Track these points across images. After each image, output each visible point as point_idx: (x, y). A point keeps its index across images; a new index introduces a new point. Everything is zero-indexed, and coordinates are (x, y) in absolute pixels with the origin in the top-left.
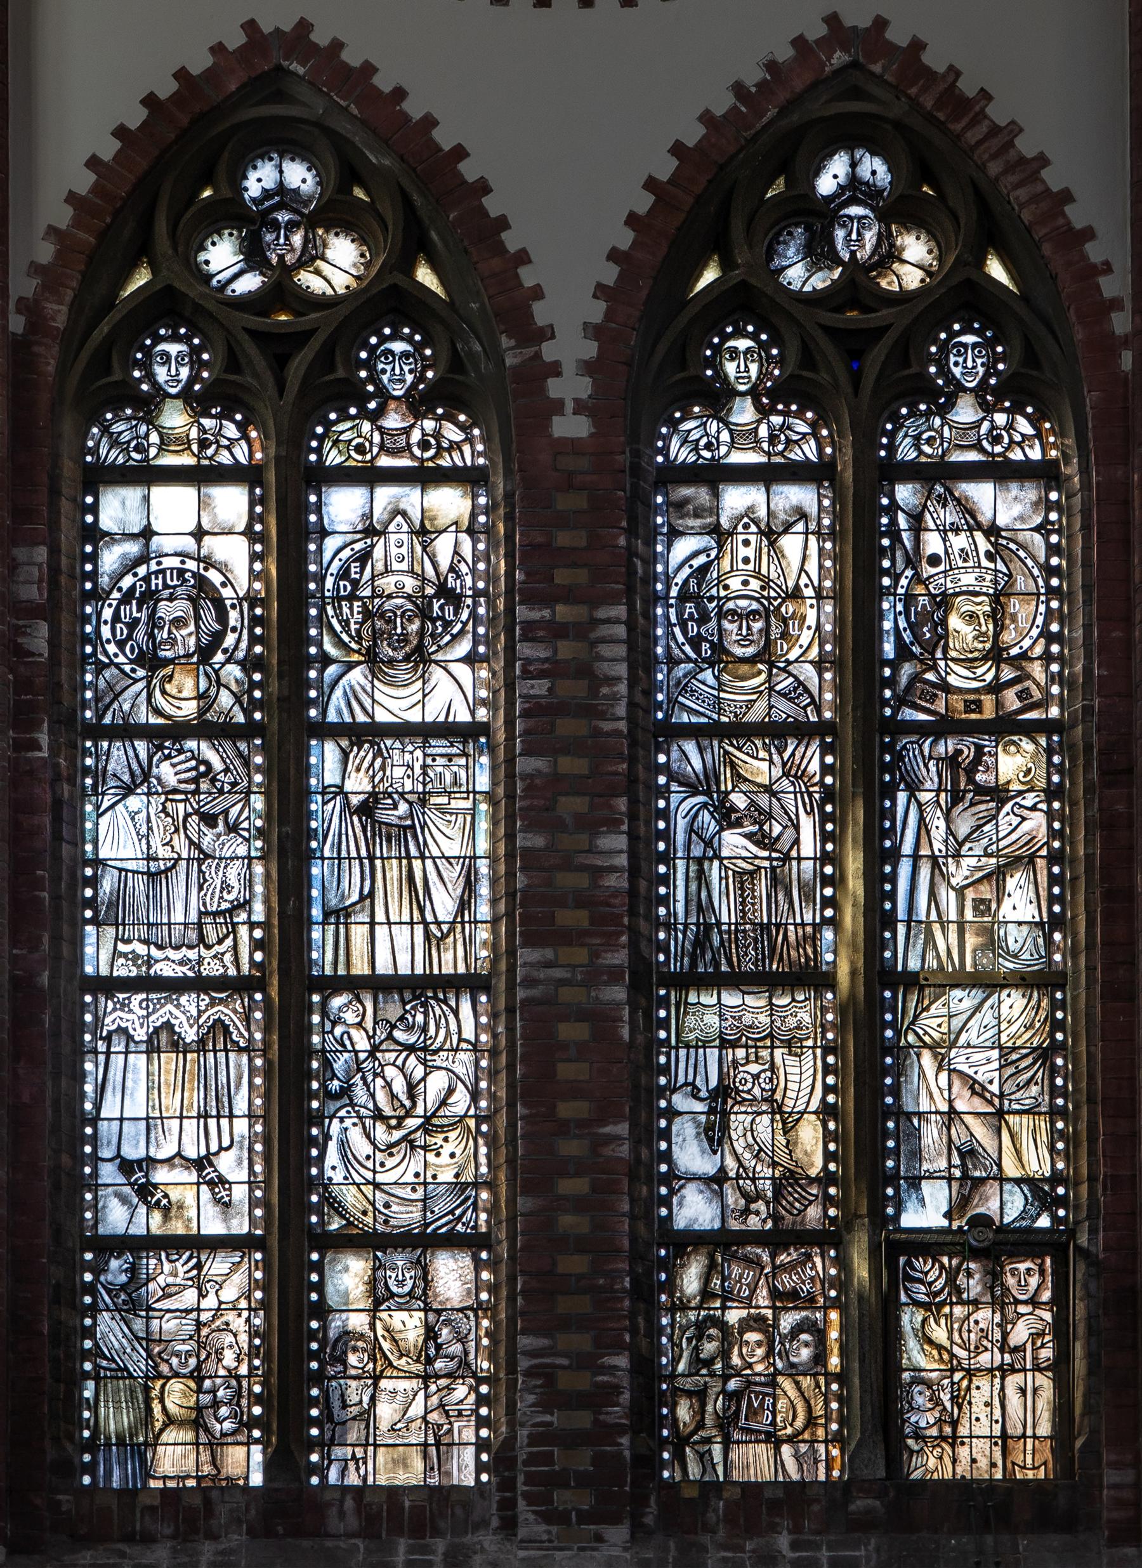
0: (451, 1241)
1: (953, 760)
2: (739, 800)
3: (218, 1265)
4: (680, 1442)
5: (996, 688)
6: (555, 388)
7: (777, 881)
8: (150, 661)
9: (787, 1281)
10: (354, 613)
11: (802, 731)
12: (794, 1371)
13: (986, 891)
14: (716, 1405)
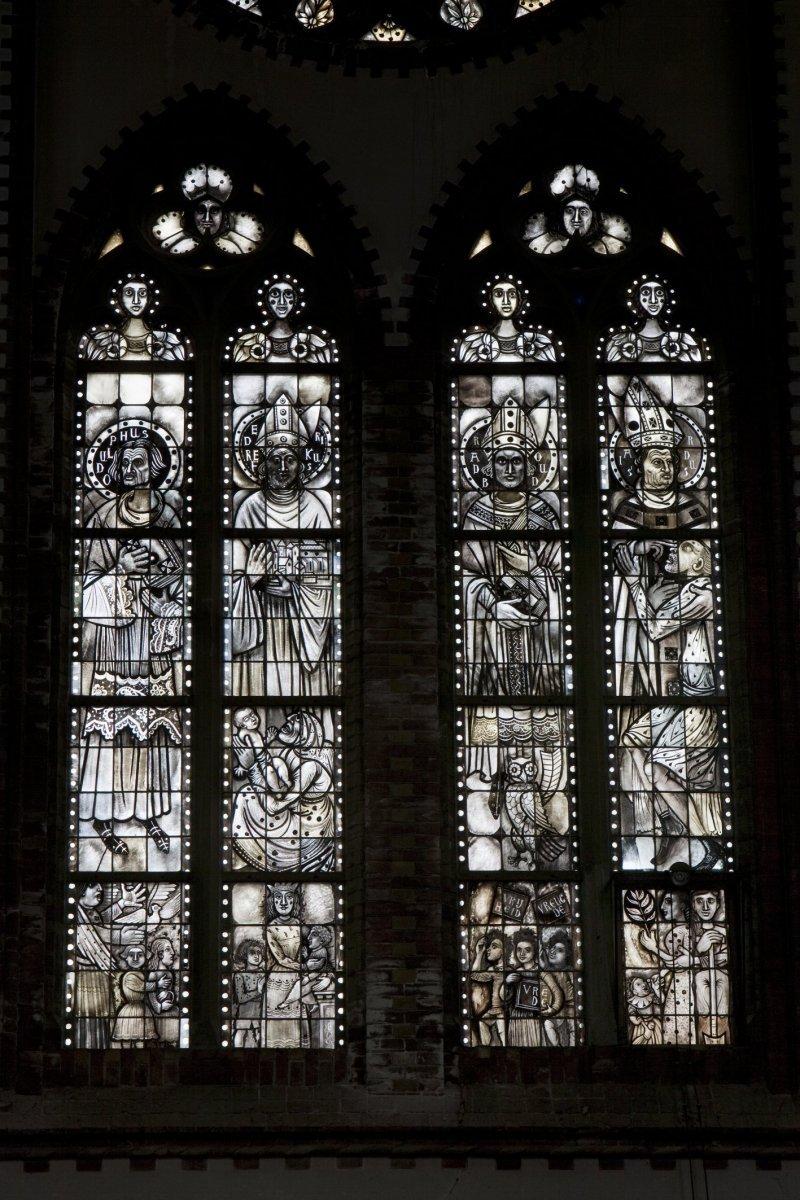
0: (318, 878)
1: (649, 557)
2: (509, 582)
3: (161, 892)
4: (475, 1018)
5: (676, 508)
6: (387, 315)
7: (535, 635)
8: (118, 486)
9: (546, 907)
10: (253, 457)
11: (550, 536)
12: (551, 969)
13: (674, 643)
14: (499, 992)
